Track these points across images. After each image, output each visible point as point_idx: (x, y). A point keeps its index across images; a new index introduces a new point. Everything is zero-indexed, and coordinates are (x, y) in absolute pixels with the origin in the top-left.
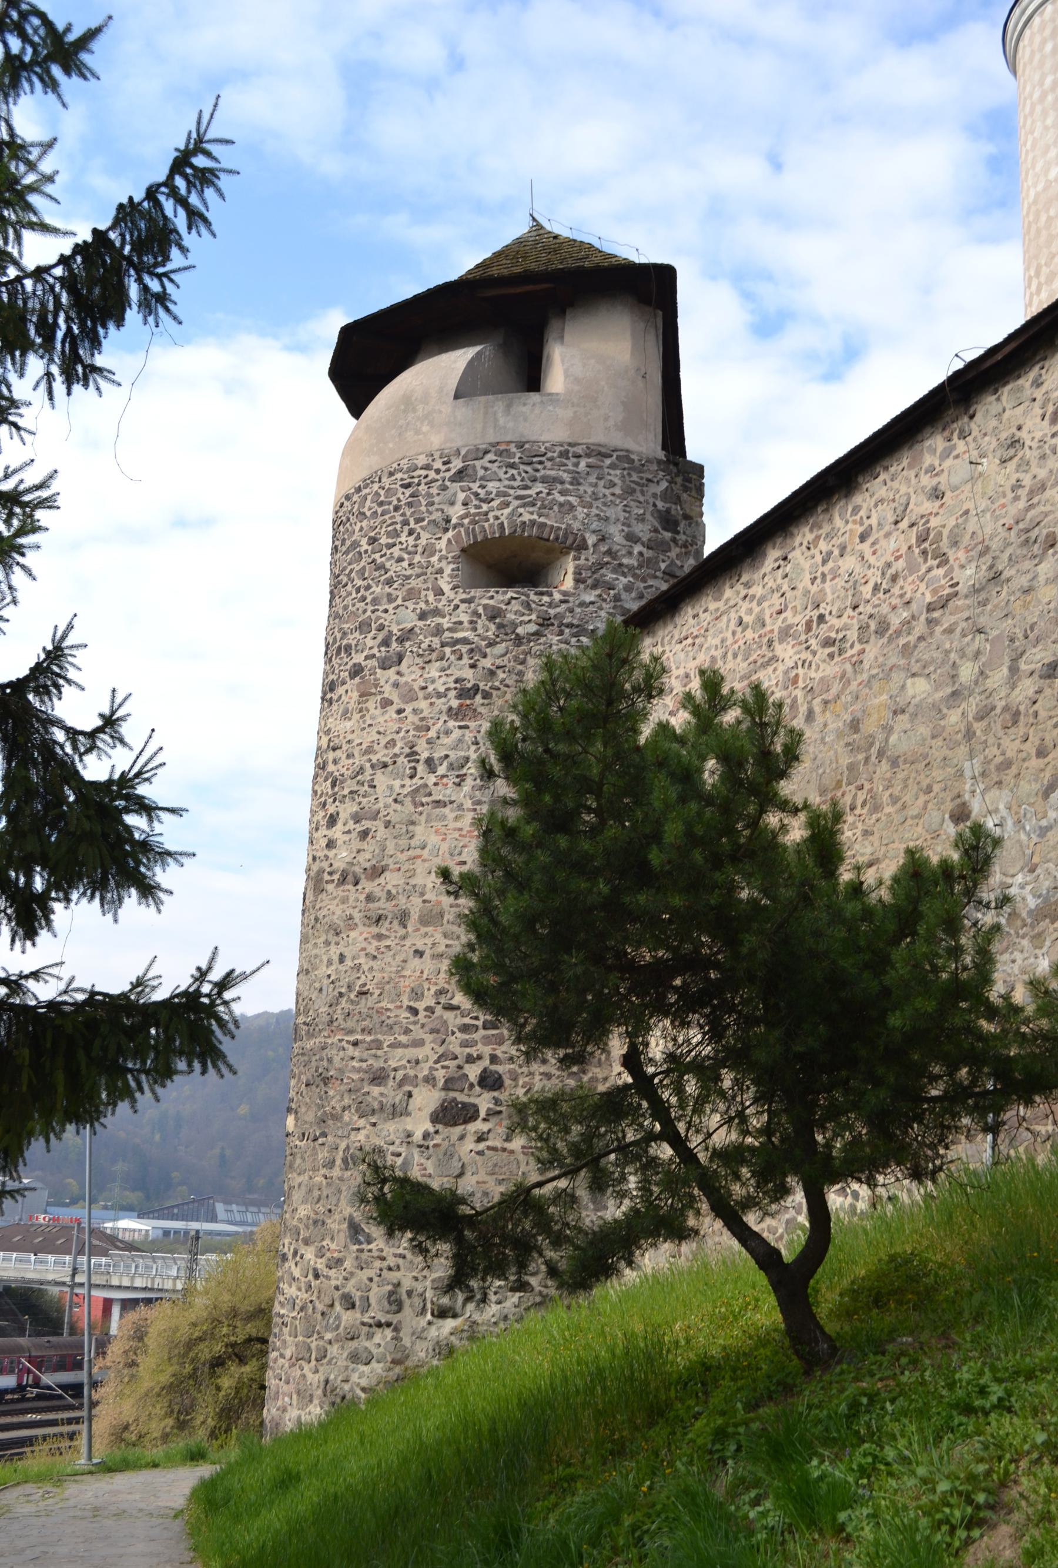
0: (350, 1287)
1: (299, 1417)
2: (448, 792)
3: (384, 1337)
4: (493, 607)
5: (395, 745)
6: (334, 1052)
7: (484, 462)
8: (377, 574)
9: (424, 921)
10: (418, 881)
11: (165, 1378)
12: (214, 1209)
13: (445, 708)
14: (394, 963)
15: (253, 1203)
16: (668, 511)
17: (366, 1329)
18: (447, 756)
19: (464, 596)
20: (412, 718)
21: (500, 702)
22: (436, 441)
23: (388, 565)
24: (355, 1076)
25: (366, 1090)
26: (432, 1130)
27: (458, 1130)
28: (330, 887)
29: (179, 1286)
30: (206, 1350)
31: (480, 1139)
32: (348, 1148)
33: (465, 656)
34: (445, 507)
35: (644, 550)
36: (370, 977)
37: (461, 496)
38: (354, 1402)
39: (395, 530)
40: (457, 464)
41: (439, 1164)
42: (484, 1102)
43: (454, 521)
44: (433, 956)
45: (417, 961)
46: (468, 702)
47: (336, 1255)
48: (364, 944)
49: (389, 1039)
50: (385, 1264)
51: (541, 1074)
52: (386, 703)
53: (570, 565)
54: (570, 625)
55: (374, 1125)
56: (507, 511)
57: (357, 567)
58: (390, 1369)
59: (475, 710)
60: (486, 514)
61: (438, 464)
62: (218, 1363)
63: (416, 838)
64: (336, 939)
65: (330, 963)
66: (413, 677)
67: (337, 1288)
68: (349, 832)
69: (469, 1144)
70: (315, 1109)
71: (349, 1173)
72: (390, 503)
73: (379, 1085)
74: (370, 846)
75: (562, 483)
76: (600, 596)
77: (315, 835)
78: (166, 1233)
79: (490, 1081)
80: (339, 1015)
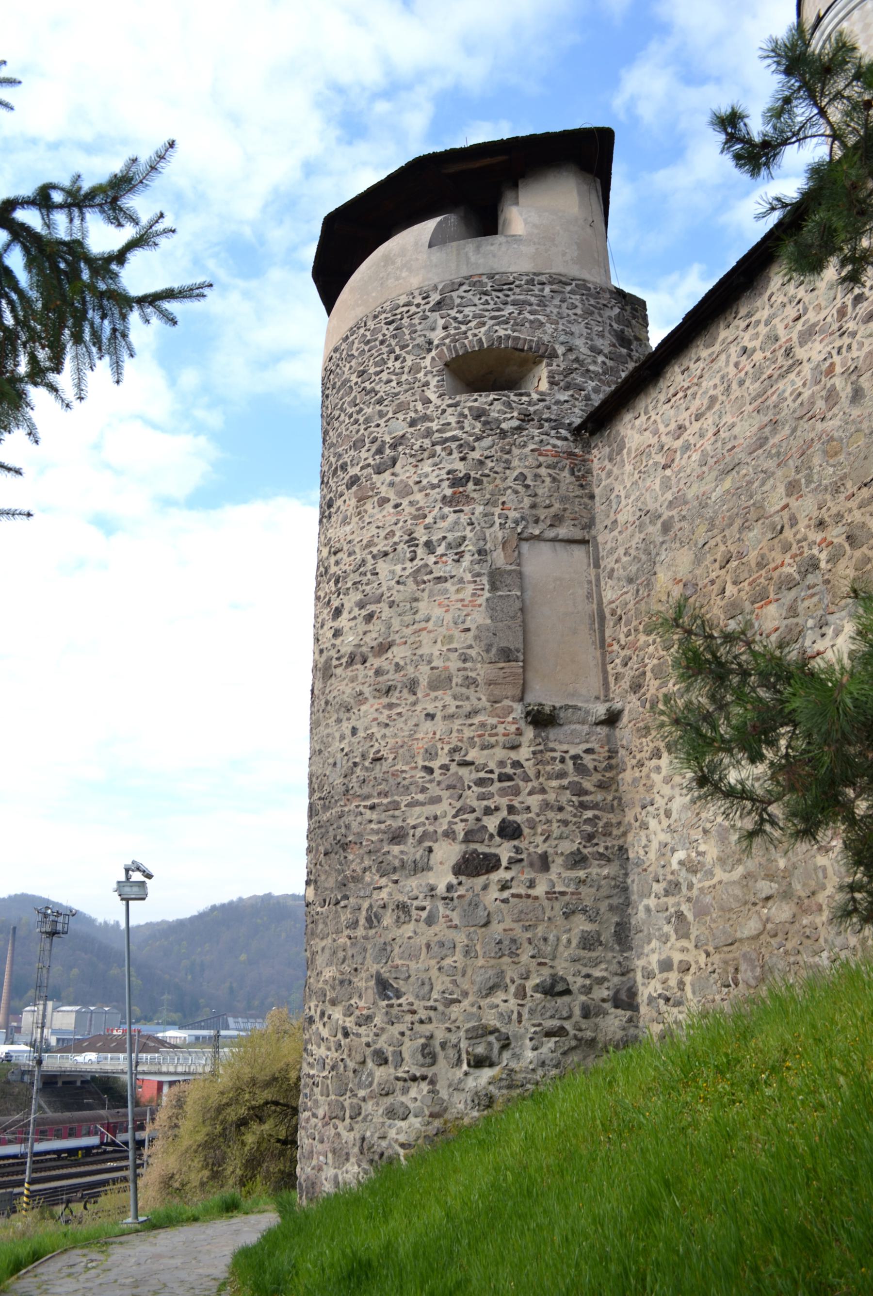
0: (382, 1043)
1: (336, 1176)
2: (448, 568)
3: (420, 1091)
4: (478, 408)
5: (394, 535)
6: (352, 818)
7: (461, 292)
8: (368, 397)
9: (434, 685)
10: (425, 650)
11: (200, 1138)
12: (227, 1021)
13: (439, 497)
14: (406, 728)
15: (252, 1016)
16: (622, 331)
17: (400, 1084)
18: (444, 538)
19: (450, 402)
20: (409, 510)
21: (491, 487)
22: (415, 282)
23: (377, 388)
24: (375, 838)
25: (386, 849)
26: (455, 882)
27: (481, 880)
28: (339, 671)
29: (208, 1069)
30: (233, 1113)
31: (504, 887)
32: (371, 906)
33: (455, 451)
34: (427, 333)
35: (607, 361)
36: (383, 743)
37: (441, 322)
38: (392, 1160)
39: (383, 359)
40: (435, 297)
41: (465, 915)
42: (505, 851)
43: (436, 342)
44: (445, 718)
45: (429, 723)
46: (461, 489)
47: (365, 1012)
48: (376, 715)
49: (405, 800)
50: (416, 1017)
51: (559, 821)
52: (384, 501)
53: (543, 372)
54: (548, 420)
55: (396, 882)
56: (483, 330)
57: (348, 399)
58: (429, 1123)
59: (468, 496)
60: (465, 333)
61: (418, 300)
62: (243, 1123)
63: (420, 613)
64: (347, 715)
65: (342, 738)
66: (408, 474)
67: (368, 1045)
68: (355, 618)
69: (494, 893)
70: (334, 874)
71: (374, 931)
72: (376, 340)
73: (398, 844)
74: (376, 626)
75: (531, 305)
76: (572, 396)
77: (321, 632)
78: (197, 1038)
79: (509, 830)
80: (354, 782)
